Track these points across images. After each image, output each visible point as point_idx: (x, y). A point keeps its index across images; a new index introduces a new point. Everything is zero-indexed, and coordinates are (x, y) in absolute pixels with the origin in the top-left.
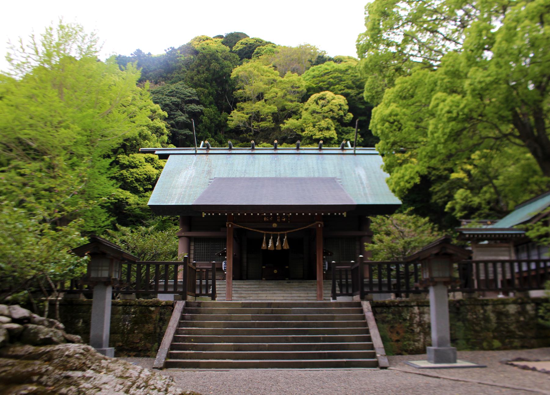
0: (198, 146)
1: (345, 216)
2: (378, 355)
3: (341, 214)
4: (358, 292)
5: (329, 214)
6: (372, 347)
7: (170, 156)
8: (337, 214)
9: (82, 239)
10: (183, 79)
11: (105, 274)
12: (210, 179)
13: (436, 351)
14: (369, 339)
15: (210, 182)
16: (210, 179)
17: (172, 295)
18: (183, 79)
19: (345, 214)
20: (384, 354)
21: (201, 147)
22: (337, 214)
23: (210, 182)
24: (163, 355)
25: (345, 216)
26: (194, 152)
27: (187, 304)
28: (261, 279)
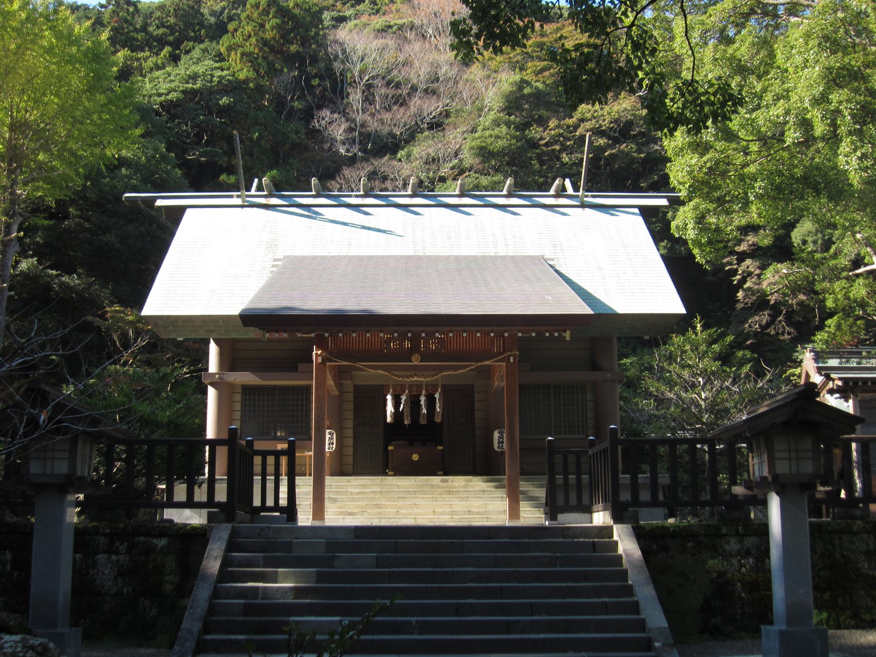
0: (248, 189)
1: (568, 338)
2: (657, 644)
3: (560, 335)
4: (859, 415)
5: (534, 334)
6: (641, 625)
7: (188, 210)
8: (552, 334)
9: (671, 521)
10: (752, 12)
11: (61, 468)
12: (275, 260)
13: (782, 634)
14: (635, 607)
15: (273, 266)
16: (275, 260)
17: (205, 512)
18: (752, 12)
19: (567, 335)
20: (671, 640)
21: (253, 192)
22: (552, 334)
23: (273, 266)
24: (188, 644)
25: (568, 338)
26: (239, 201)
27: (234, 534)
28: (386, 474)
